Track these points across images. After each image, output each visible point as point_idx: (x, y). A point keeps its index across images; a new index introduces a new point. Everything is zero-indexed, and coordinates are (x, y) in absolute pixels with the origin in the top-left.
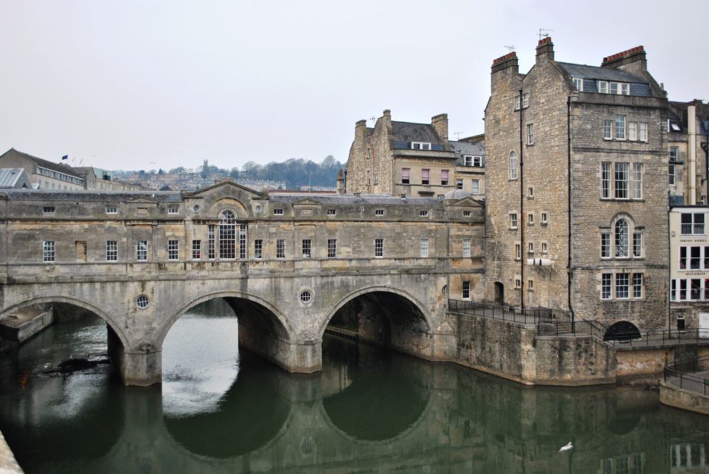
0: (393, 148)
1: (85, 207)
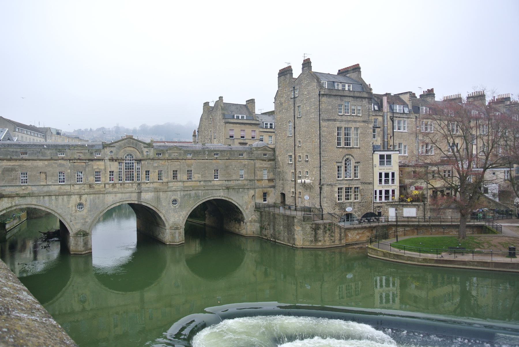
0: (224, 118)
1: (45, 152)
